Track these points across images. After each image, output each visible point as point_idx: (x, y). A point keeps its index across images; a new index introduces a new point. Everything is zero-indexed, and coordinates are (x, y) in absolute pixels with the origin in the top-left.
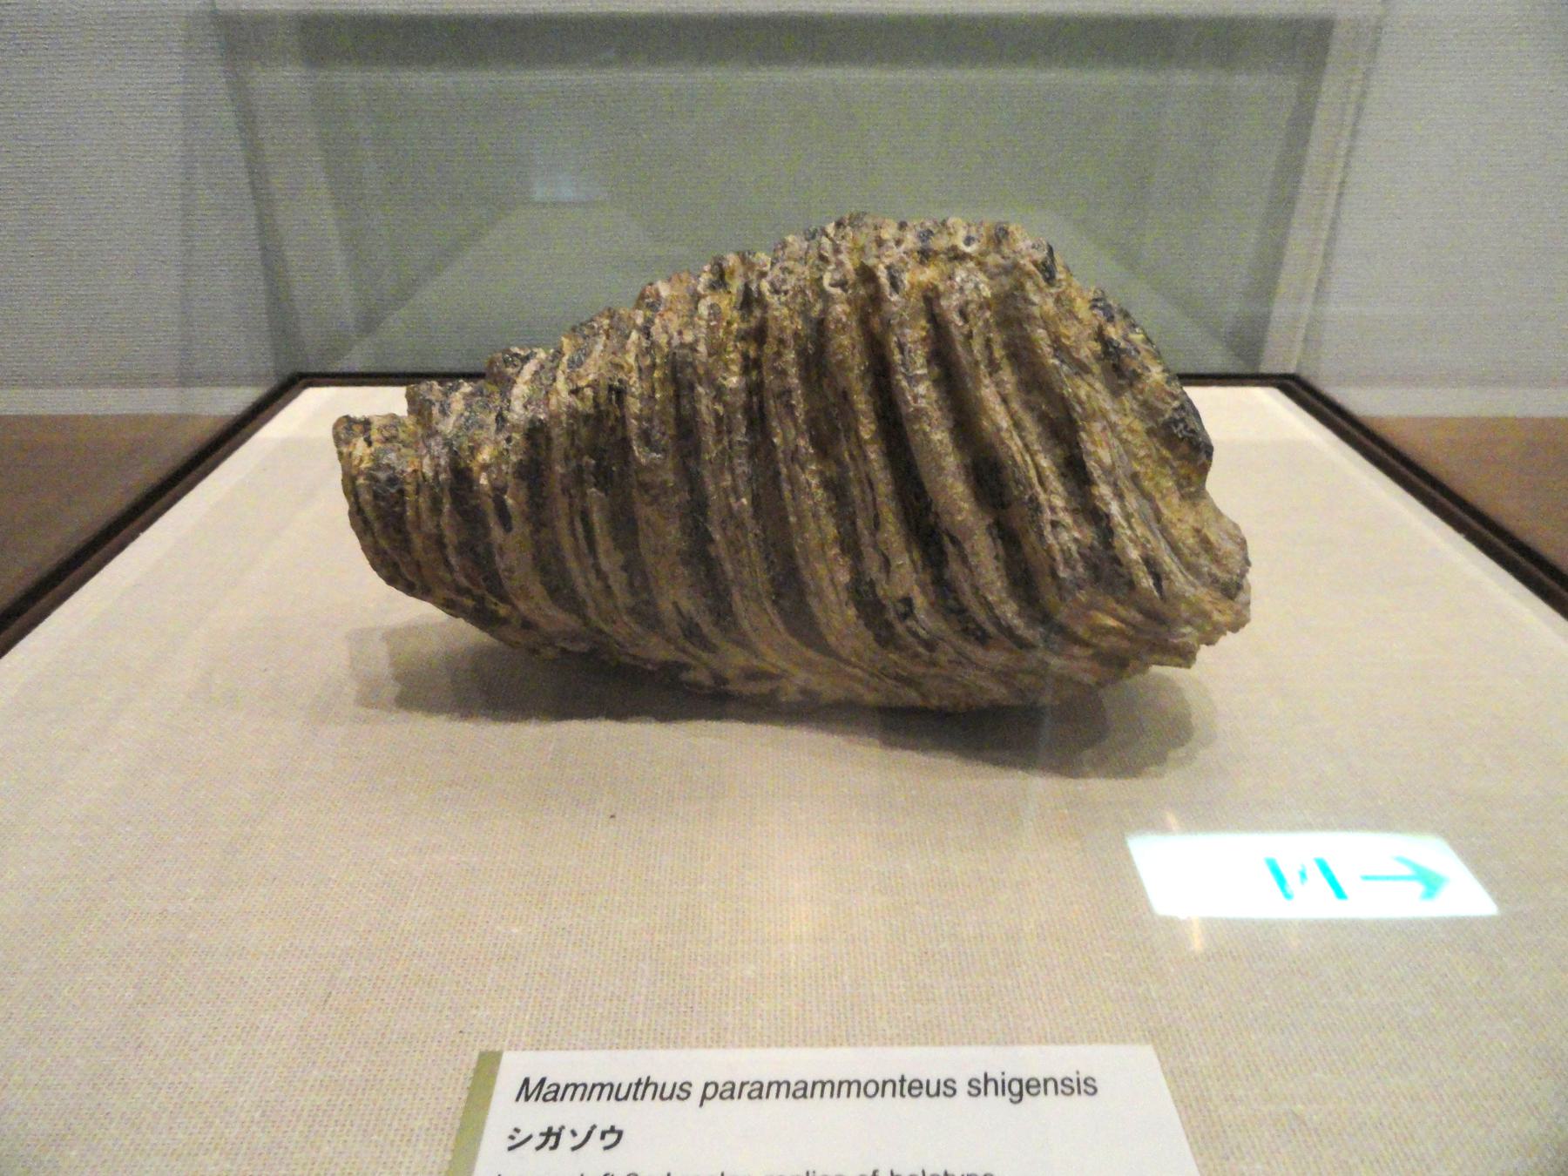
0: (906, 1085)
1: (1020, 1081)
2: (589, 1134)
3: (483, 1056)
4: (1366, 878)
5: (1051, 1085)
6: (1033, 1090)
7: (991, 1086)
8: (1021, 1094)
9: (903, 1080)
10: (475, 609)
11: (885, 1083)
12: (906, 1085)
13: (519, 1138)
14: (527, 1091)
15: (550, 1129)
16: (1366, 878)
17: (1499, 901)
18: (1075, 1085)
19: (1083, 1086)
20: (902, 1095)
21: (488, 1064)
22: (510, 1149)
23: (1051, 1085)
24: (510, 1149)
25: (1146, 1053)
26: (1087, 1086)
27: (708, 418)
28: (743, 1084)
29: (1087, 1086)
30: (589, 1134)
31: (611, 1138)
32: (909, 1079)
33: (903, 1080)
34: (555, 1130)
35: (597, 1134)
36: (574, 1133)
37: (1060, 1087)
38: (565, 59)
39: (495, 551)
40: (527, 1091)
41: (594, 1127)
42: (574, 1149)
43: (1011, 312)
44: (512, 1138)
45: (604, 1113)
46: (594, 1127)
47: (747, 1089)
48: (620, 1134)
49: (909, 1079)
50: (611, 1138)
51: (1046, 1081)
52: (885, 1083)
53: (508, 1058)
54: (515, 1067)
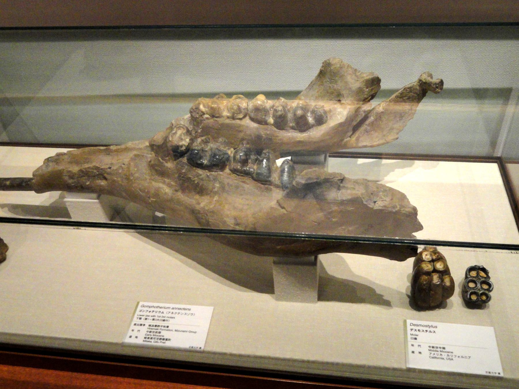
21: (138, 303)
40: (143, 306)
54: (141, 303)
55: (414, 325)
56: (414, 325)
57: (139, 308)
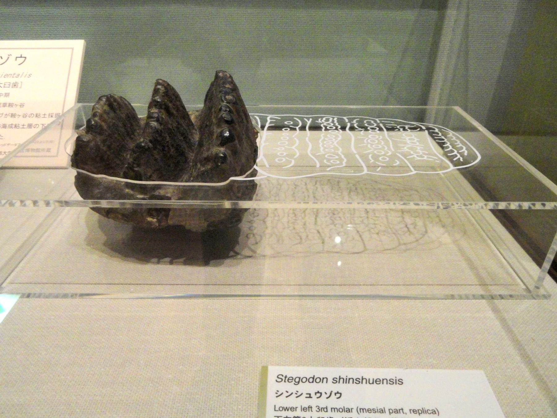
0: (287, 379)
1: (300, 378)
2: (331, 394)
3: (263, 367)
5: (385, 381)
6: (378, 383)
7: (342, 380)
8: (299, 382)
9: (286, 377)
11: (323, 378)
12: (287, 379)
13: (279, 393)
14: (282, 379)
18: (394, 381)
19: (398, 382)
20: (285, 382)
22: (277, 397)
23: (385, 381)
24: (277, 397)
25: (482, 372)
26: (400, 382)
27: (446, 107)
29: (400, 382)
30: (331, 394)
31: (338, 395)
32: (288, 376)
33: (286, 377)
35: (333, 394)
36: (326, 393)
37: (389, 382)
39: (123, 207)
40: (282, 379)
42: (287, 397)
43: (234, 94)
44: (277, 393)
45: (336, 388)
48: (341, 394)
49: (288, 376)
50: (338, 395)
51: (383, 380)
53: (270, 368)
54: (273, 371)
55: (289, 379)
56: (289, 379)
57: (272, 386)
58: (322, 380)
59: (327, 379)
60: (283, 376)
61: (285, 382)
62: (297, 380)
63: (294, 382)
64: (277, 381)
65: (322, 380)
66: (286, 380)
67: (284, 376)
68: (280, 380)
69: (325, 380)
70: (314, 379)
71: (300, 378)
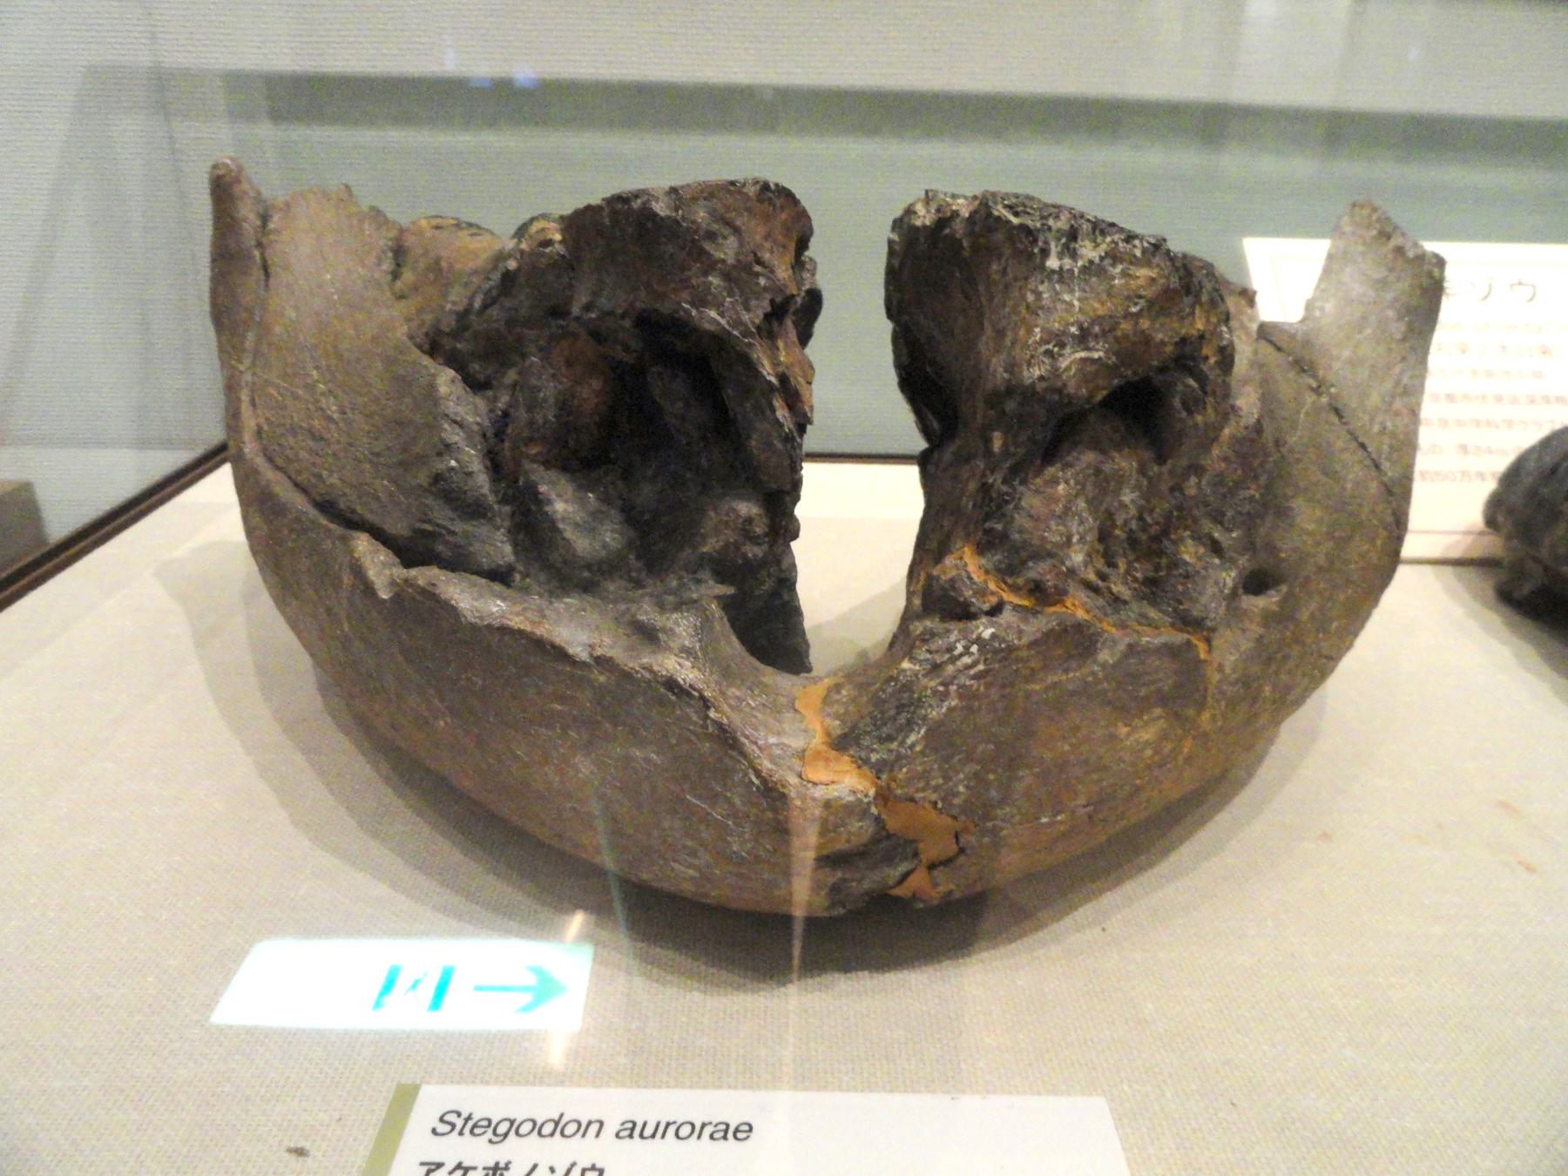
0: (470, 1124)
4: (479, 988)
10: (1196, 474)
12: (470, 1124)
14: (454, 1123)
15: (497, 1164)
16: (479, 988)
17: (222, 1030)
21: (404, 1099)
26: (743, 1132)
28: (703, 1126)
29: (743, 1132)
32: (476, 1117)
34: (502, 1165)
38: (931, 133)
40: (454, 1123)
41: (573, 1165)
46: (573, 1165)
47: (708, 1130)
49: (476, 1117)
52: (590, 1123)
53: (426, 1091)
54: (432, 1101)
55: (473, 1126)
56: (473, 1126)
58: (582, 1128)
59: (601, 1123)
60: (459, 1115)
61: (461, 1133)
62: (502, 1129)
63: (490, 1134)
64: (434, 1131)
65: (582, 1128)
66: (467, 1130)
67: (465, 1115)
68: (448, 1128)
69: (594, 1128)
70: (558, 1126)
71: (512, 1122)
